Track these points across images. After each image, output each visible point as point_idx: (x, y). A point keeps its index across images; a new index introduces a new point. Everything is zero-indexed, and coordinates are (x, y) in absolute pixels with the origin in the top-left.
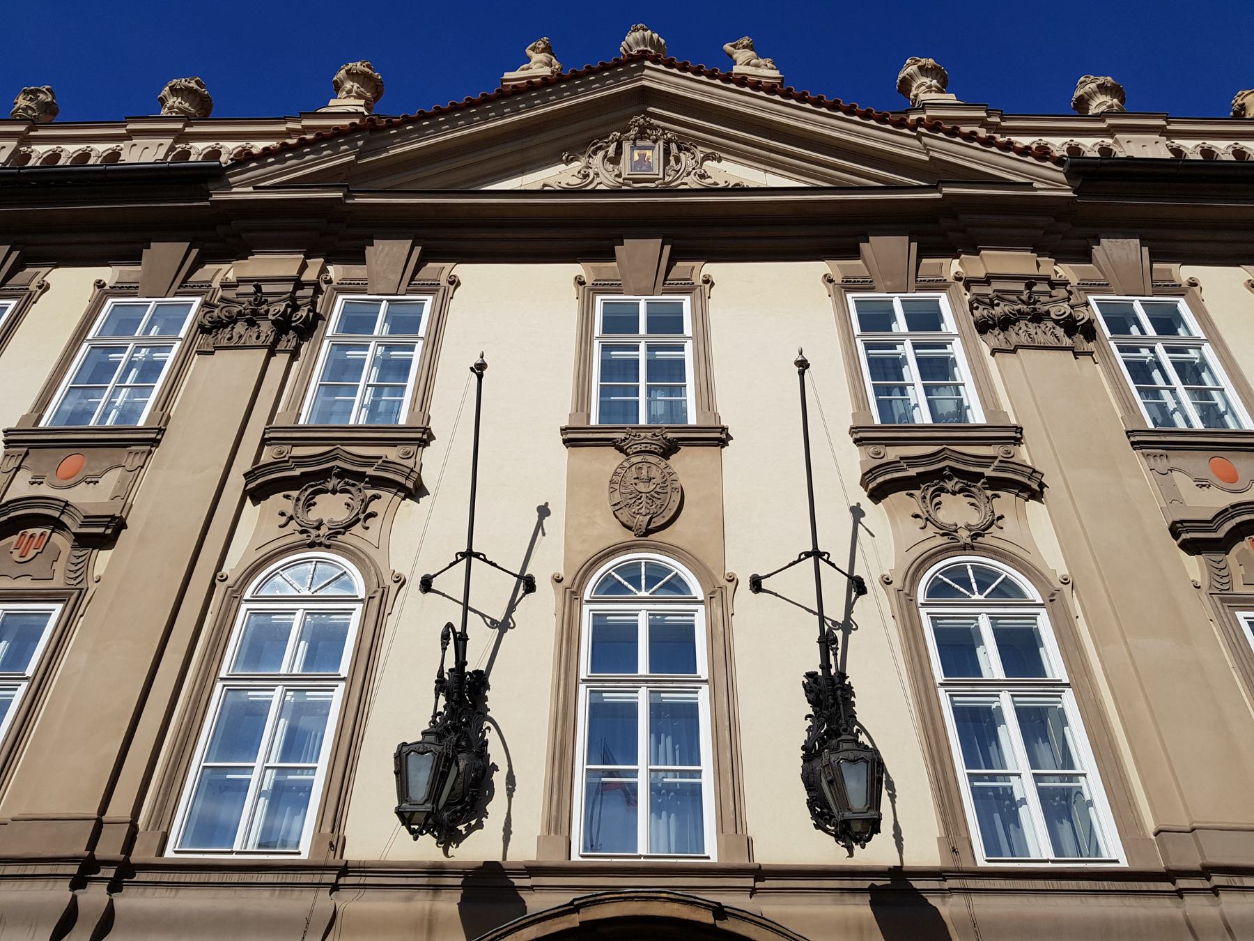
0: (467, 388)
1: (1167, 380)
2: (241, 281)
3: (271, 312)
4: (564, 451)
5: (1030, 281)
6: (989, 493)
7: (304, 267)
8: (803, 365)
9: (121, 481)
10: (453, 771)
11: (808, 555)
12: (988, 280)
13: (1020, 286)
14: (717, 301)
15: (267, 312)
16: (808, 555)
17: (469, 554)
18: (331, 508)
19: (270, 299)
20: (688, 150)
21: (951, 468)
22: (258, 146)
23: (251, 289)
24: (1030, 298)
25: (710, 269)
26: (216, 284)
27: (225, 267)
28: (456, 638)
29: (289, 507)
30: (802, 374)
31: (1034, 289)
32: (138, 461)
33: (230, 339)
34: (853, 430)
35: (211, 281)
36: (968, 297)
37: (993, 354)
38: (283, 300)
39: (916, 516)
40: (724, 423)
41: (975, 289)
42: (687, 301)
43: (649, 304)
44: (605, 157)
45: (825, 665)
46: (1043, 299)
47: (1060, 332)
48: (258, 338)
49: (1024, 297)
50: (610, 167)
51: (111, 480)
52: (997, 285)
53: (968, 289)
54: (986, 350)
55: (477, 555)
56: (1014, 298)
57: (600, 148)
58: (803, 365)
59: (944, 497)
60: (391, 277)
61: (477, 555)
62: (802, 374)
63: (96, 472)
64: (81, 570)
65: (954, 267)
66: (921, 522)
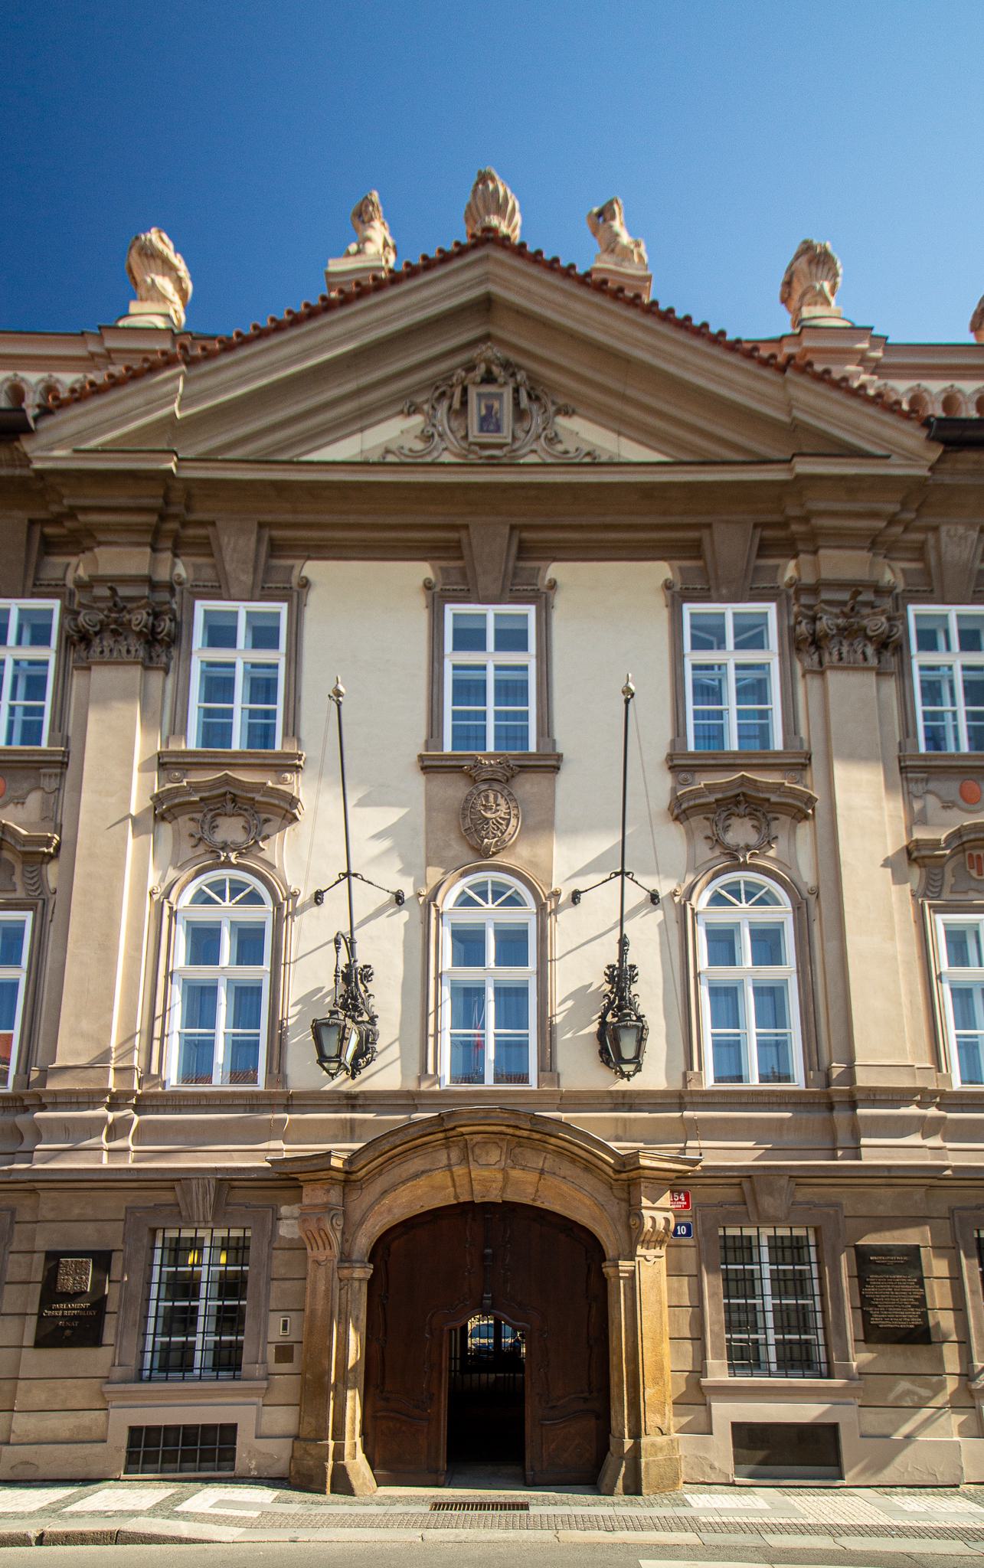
0: (329, 712)
1: (953, 704)
2: (96, 580)
3: (134, 622)
4: (421, 779)
5: (855, 587)
6: (771, 816)
7: (154, 563)
8: (629, 695)
9: (45, 803)
10: (617, 1029)
11: (617, 874)
12: (814, 590)
13: (845, 596)
14: (315, 604)
15: (130, 621)
16: (617, 874)
17: (348, 875)
18: (231, 829)
19: (129, 606)
20: (538, 399)
21: (744, 794)
22: (68, 379)
23: (103, 591)
24: (852, 609)
25: (556, 570)
26: (70, 585)
27: (73, 560)
28: (346, 942)
29: (192, 827)
30: (627, 701)
31: (860, 598)
32: (54, 784)
33: (102, 652)
34: (670, 757)
35: (64, 579)
36: (795, 609)
37: (804, 676)
38: (143, 607)
39: (192, 836)
40: (559, 750)
41: (805, 600)
42: (530, 610)
43: (498, 617)
44: (450, 407)
45: (621, 960)
46: (866, 611)
47: (870, 650)
48: (128, 651)
49: (847, 609)
50: (455, 424)
51: (34, 799)
52: (826, 595)
53: (797, 599)
54: (799, 671)
55: (355, 875)
56: (836, 610)
57: (443, 394)
58: (629, 695)
59: (735, 821)
60: (243, 578)
61: (355, 875)
62: (627, 701)
63: (20, 793)
64: (40, 881)
65: (790, 570)
66: (193, 842)
